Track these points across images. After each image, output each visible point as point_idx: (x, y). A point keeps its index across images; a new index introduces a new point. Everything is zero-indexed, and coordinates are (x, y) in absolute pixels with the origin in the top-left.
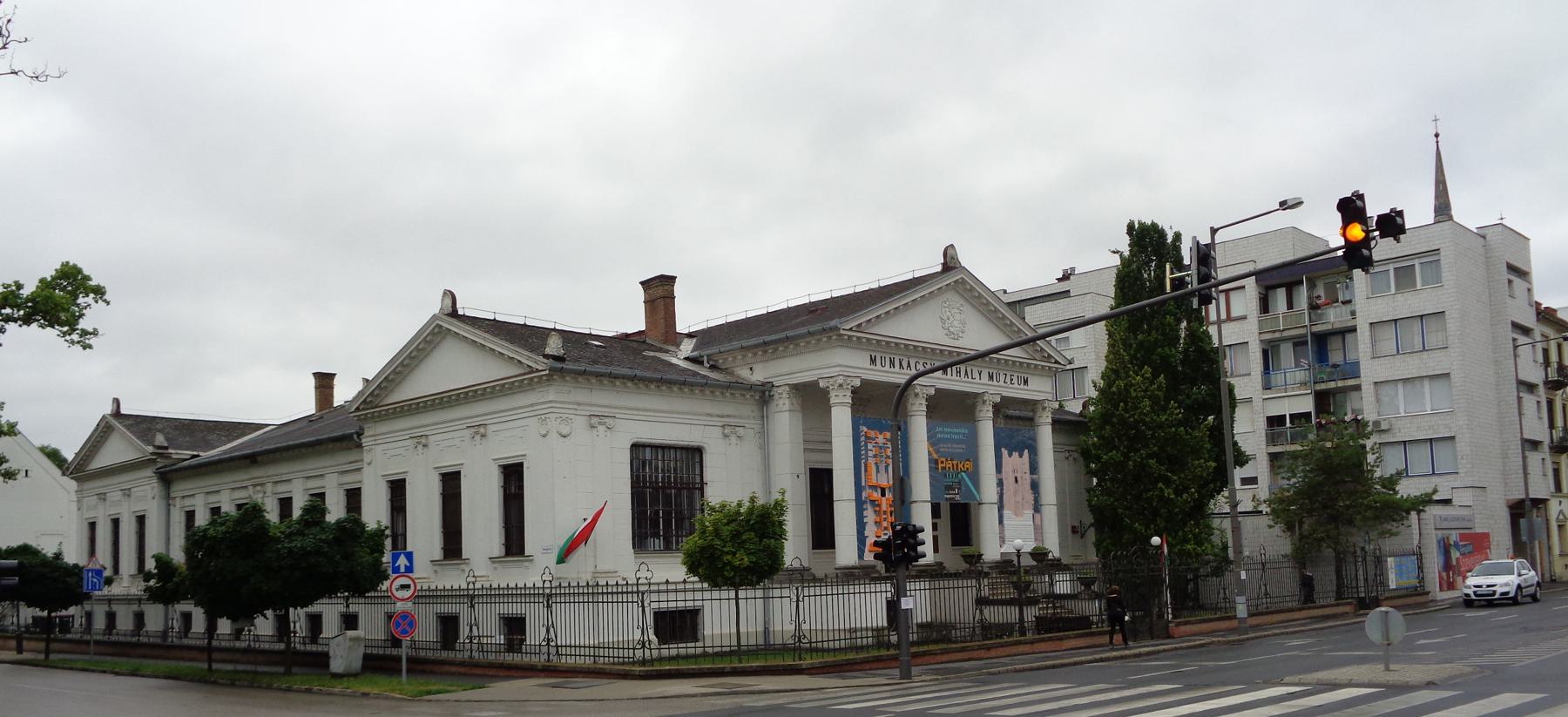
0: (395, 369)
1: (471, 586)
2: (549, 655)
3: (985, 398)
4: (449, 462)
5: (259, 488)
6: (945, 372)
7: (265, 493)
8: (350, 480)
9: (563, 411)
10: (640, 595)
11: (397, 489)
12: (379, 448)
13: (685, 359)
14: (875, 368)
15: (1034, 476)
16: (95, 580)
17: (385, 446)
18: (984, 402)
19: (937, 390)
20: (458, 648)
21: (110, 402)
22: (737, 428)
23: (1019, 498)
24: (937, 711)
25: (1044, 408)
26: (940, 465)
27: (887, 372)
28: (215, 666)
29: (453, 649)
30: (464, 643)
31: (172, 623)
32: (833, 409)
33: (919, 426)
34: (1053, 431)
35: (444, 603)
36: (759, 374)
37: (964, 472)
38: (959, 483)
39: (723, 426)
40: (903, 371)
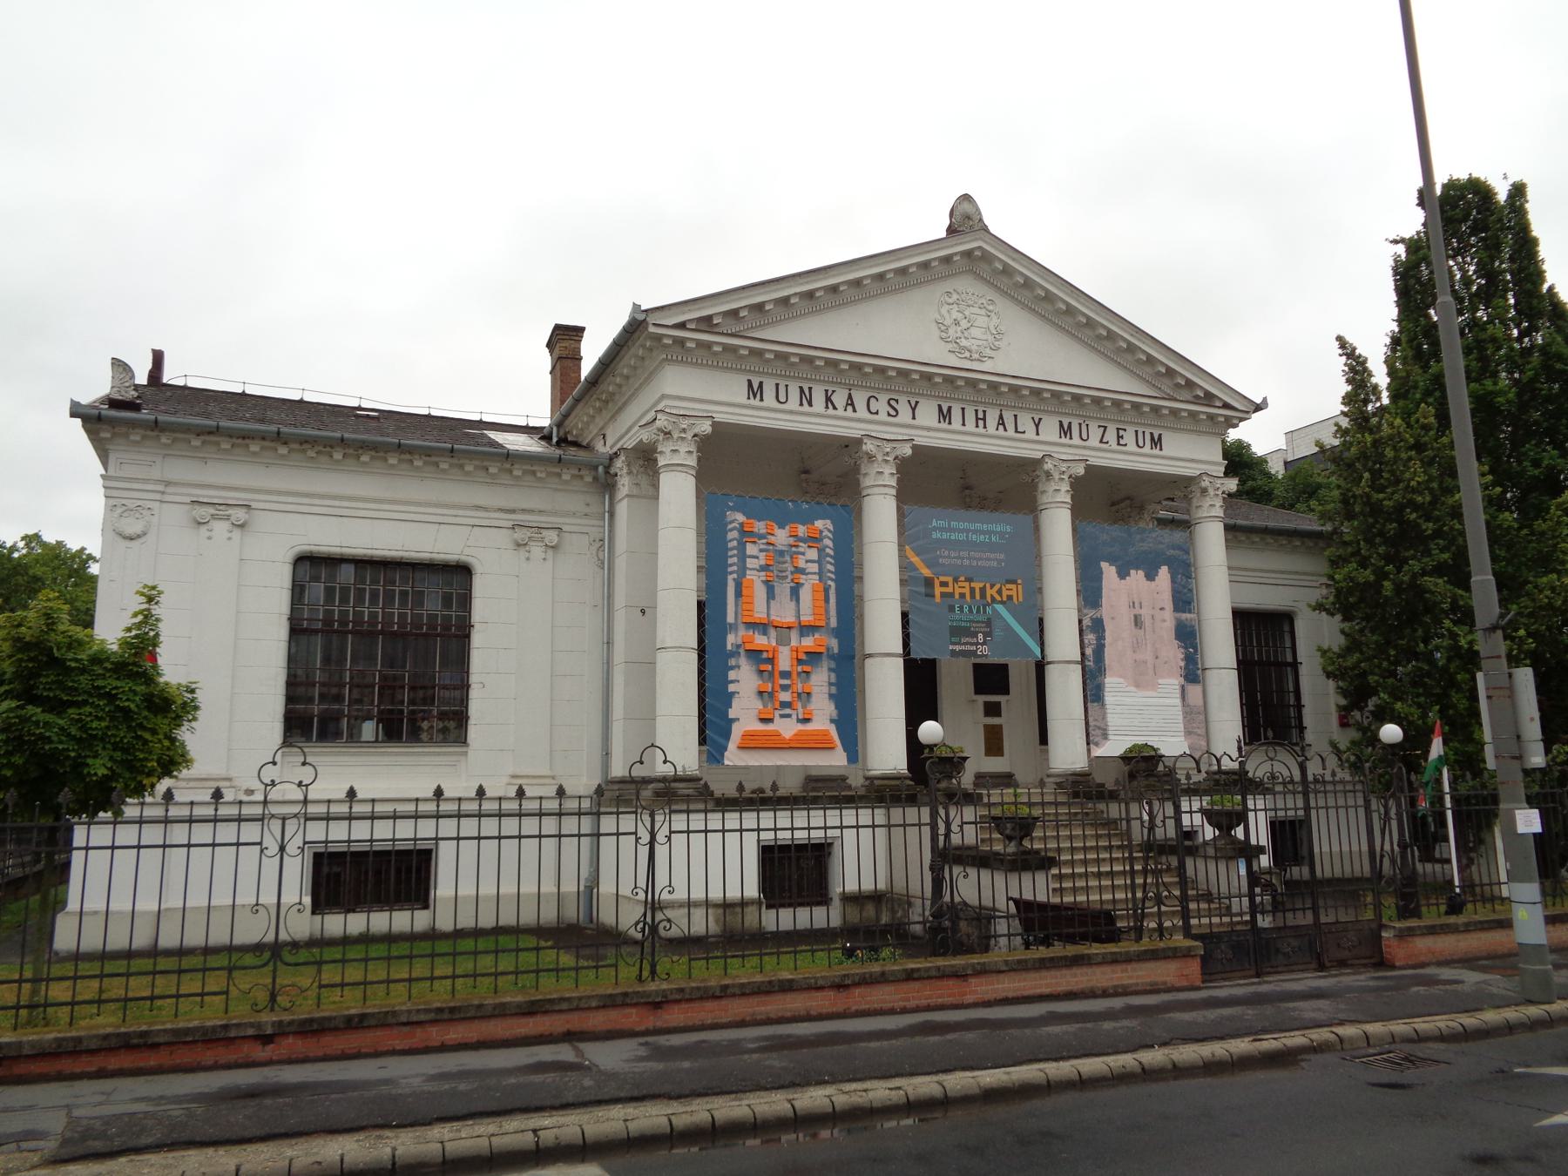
3: (1203, 484)
9: (145, 496)
14: (1071, 442)
15: (1185, 616)
19: (1089, 469)
23: (1148, 655)
26: (938, 590)
27: (791, 412)
37: (1002, 602)
38: (989, 623)
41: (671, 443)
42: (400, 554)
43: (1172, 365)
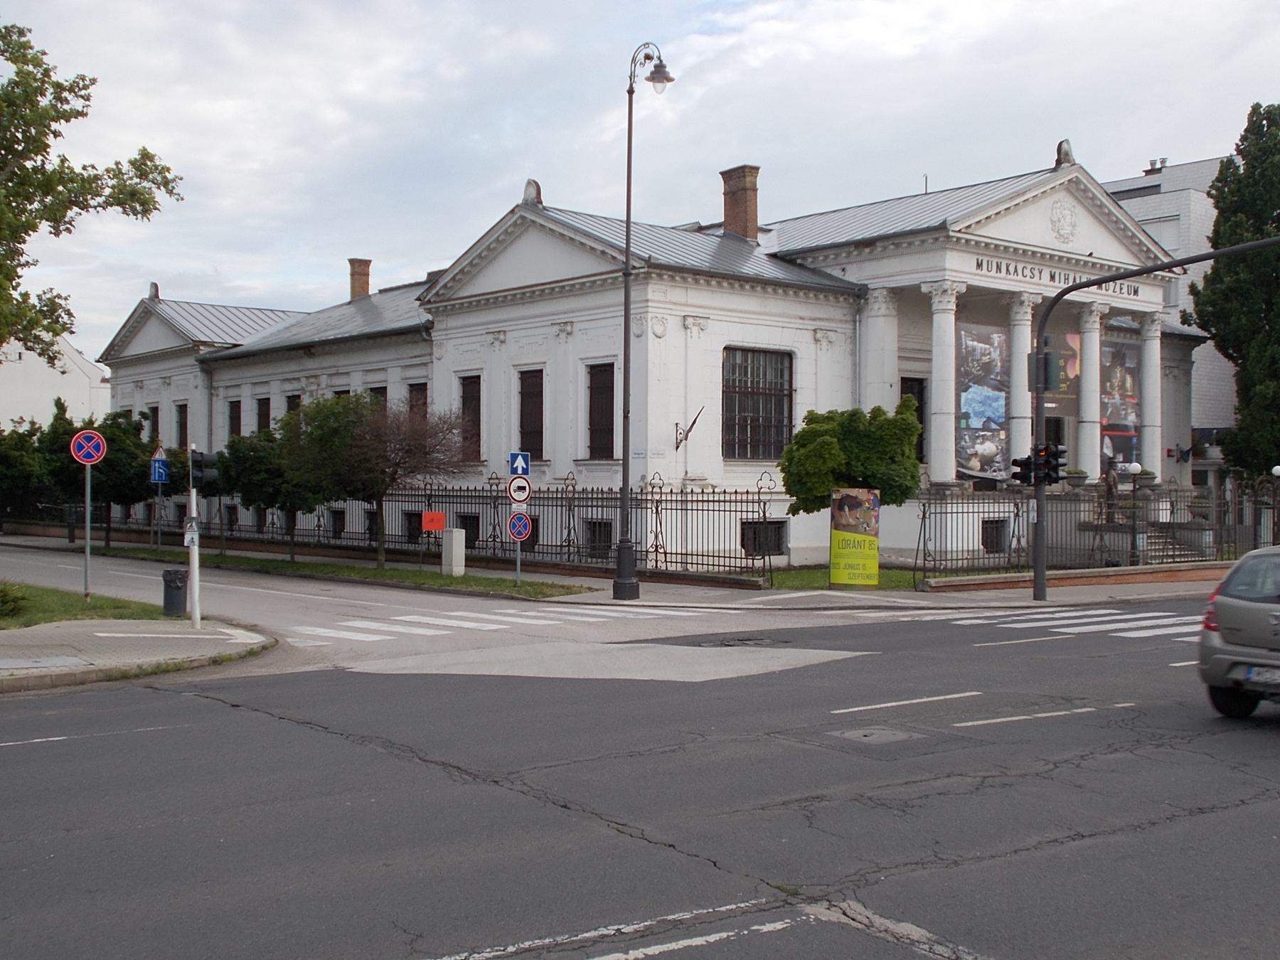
0: (471, 261)
1: (494, 487)
2: (657, 562)
4: (530, 361)
5: (312, 380)
6: (1100, 287)
7: (319, 385)
8: (416, 375)
10: (762, 504)
11: (471, 386)
12: (452, 342)
13: (773, 256)
16: (161, 471)
17: (459, 341)
18: (1091, 312)
20: (536, 550)
21: (148, 287)
22: (828, 332)
24: (958, 623)
25: (1153, 321)
28: (113, 544)
29: (340, 538)
30: (487, 541)
31: (273, 519)
32: (935, 316)
33: (945, 323)
34: (1162, 343)
35: (460, 503)
36: (854, 275)
39: (815, 331)
40: (1009, 277)
41: (946, 297)
42: (754, 345)
43: (1150, 246)
